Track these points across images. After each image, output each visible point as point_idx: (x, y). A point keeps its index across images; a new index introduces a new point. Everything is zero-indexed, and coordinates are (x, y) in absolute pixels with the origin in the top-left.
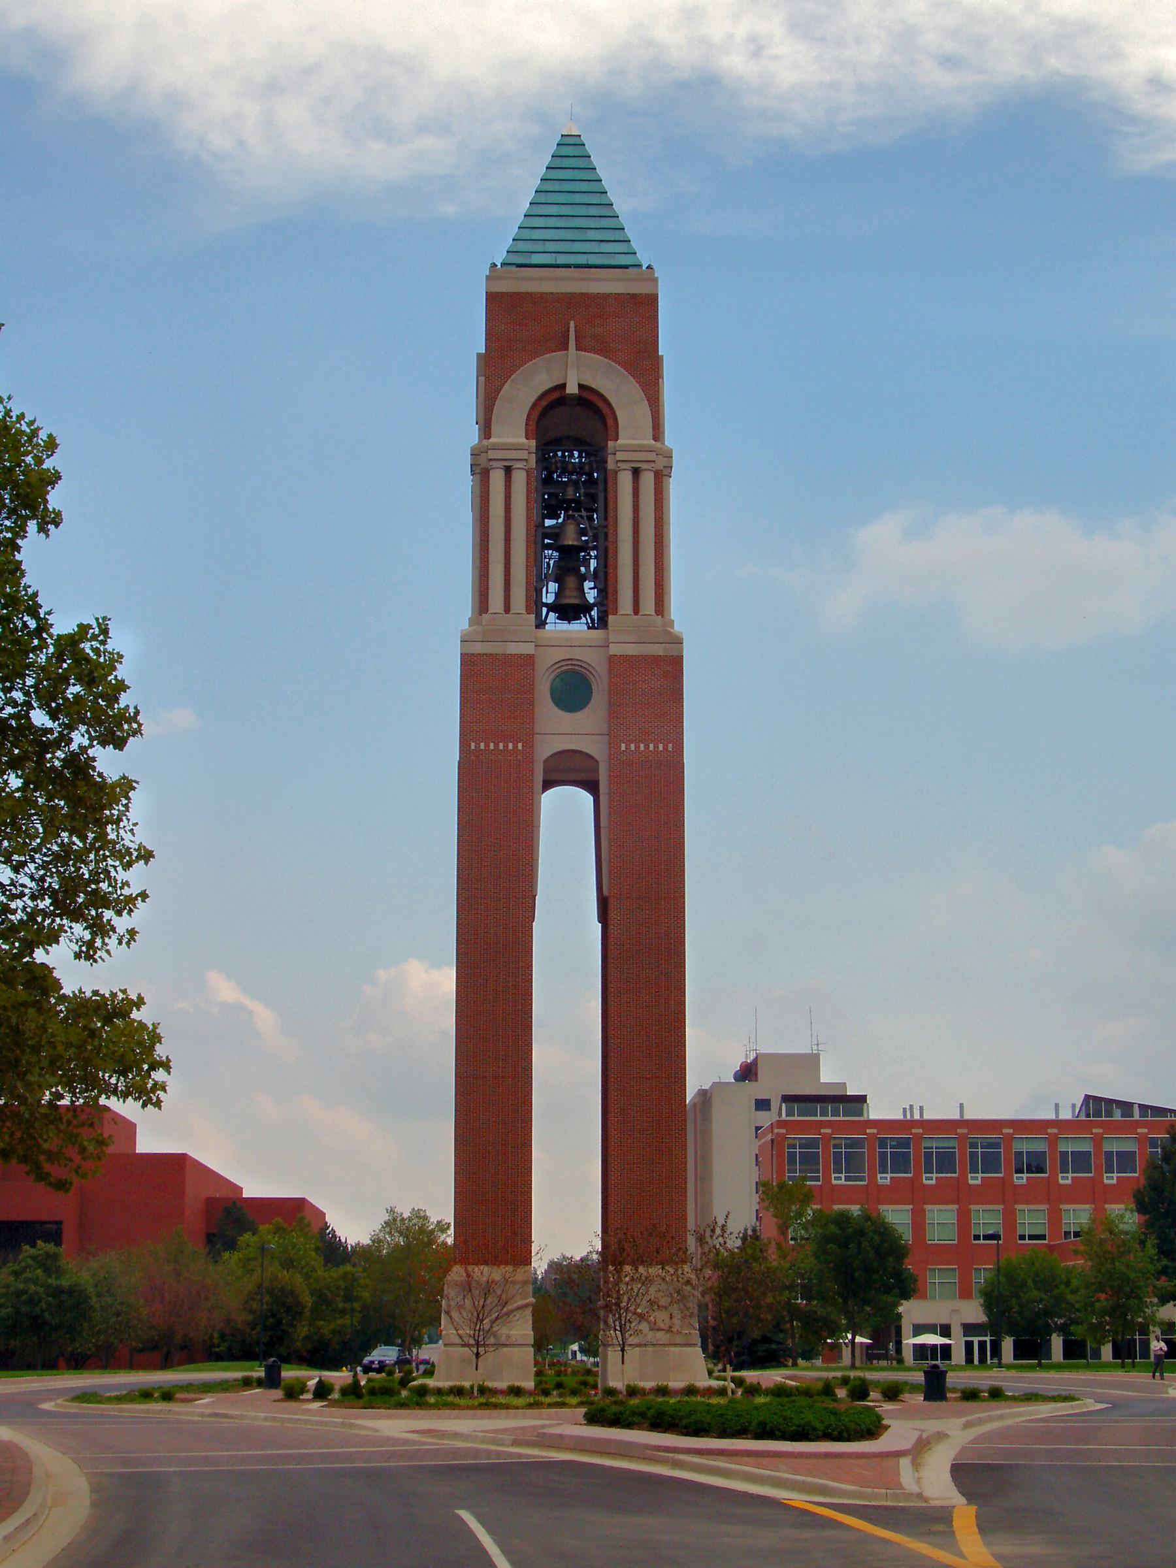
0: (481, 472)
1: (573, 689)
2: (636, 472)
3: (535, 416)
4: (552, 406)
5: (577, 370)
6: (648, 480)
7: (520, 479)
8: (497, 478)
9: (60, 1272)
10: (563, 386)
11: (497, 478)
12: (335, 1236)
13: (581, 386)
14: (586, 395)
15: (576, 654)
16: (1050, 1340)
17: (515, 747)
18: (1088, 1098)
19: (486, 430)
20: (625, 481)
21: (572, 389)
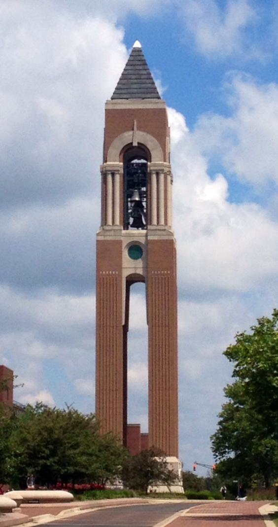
0: (104, 175)
1: (136, 250)
2: (158, 174)
3: (125, 149)
4: (128, 149)
5: (137, 137)
6: (162, 177)
7: (118, 178)
8: (110, 178)
9: (274, 318)
10: (132, 143)
11: (110, 178)
12: (78, 415)
13: (138, 143)
14: (140, 146)
15: (135, 239)
16: (96, 411)
17: (106, 272)
18: (139, 425)
19: (105, 160)
20: (154, 177)
21: (135, 144)
